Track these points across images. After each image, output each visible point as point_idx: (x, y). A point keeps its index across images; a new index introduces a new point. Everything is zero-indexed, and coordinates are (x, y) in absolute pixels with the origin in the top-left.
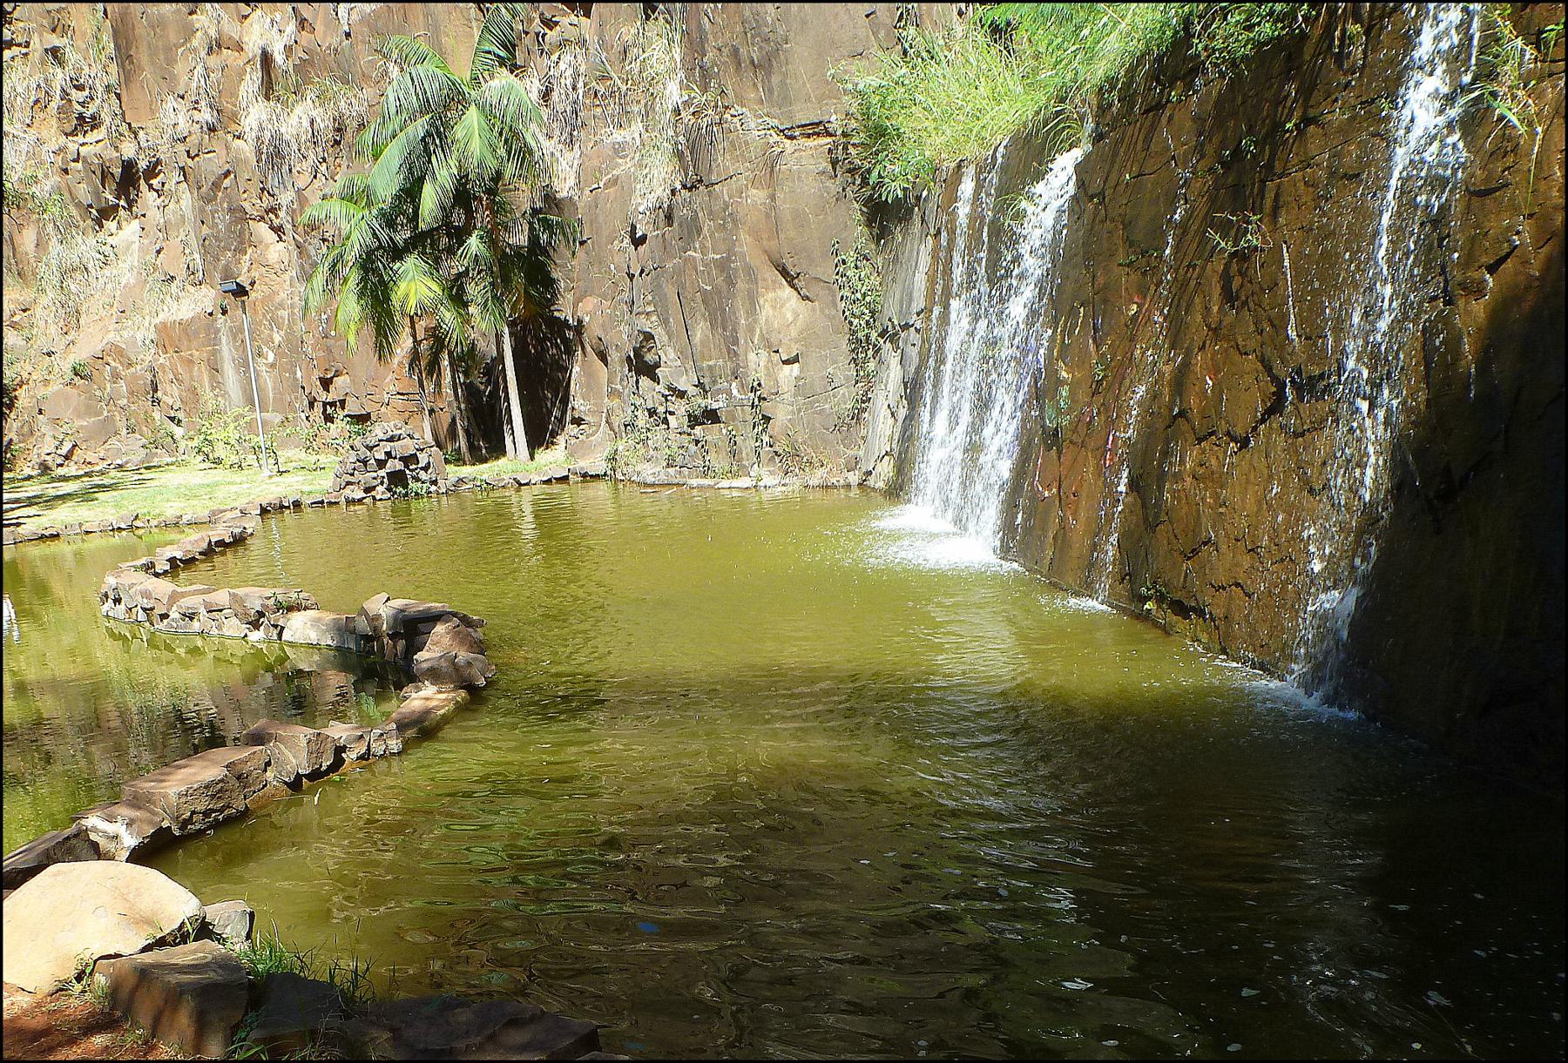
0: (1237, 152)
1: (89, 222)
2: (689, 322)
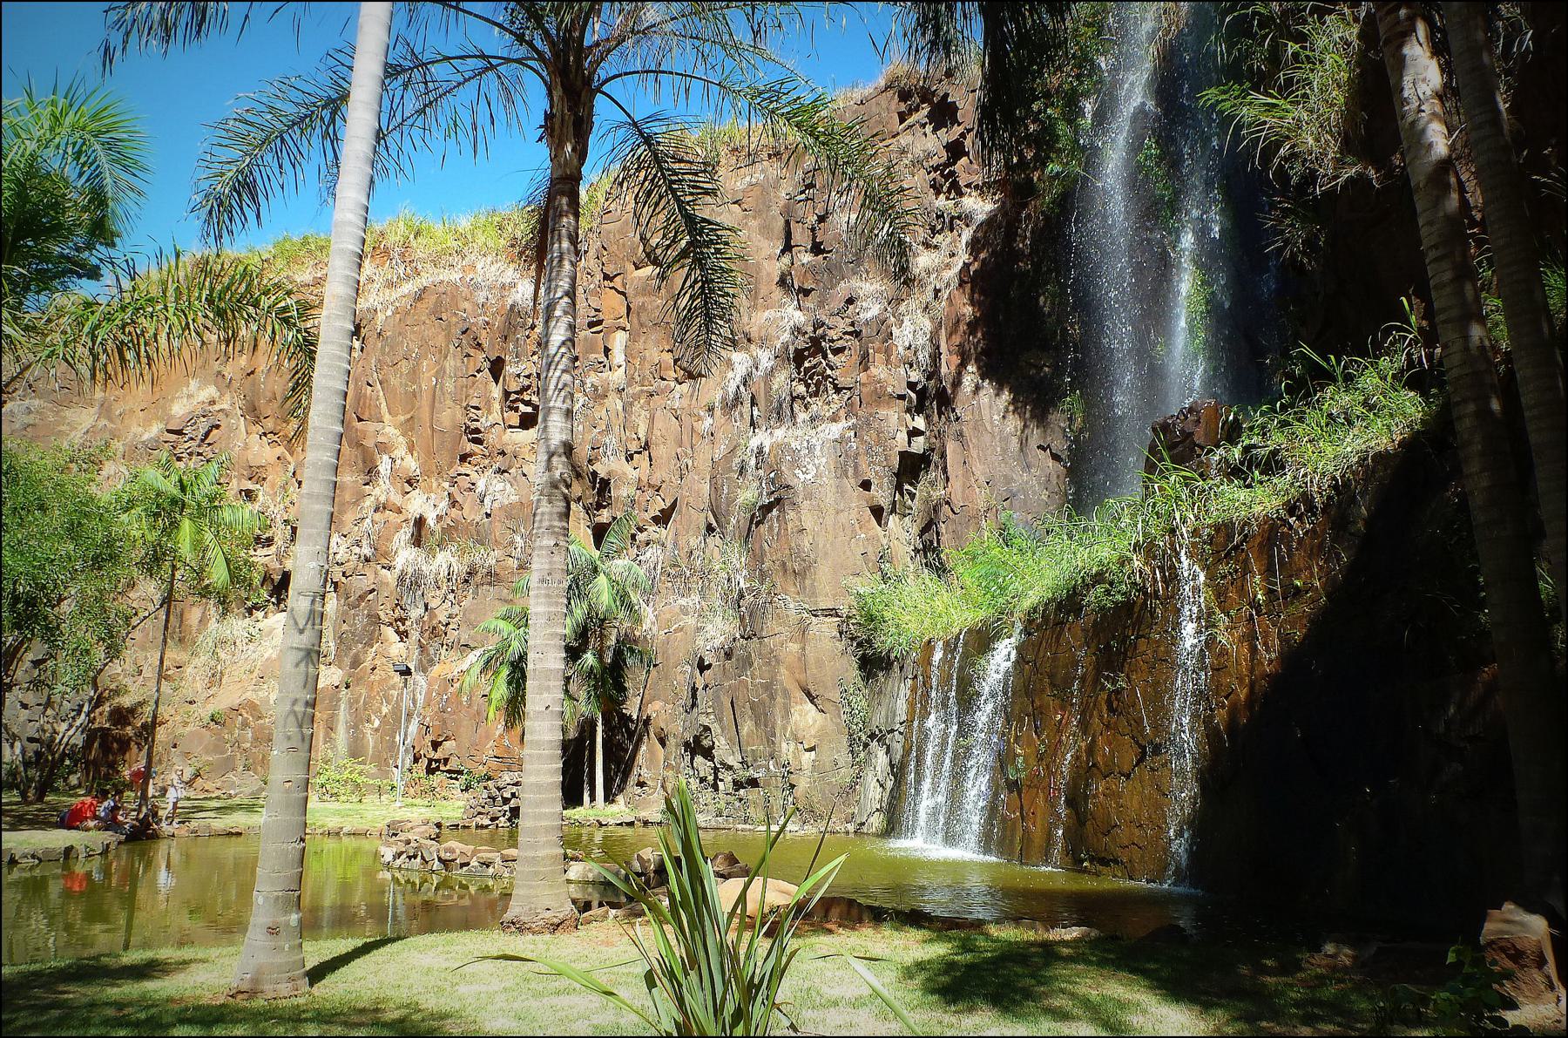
1: (242, 610)
2: (738, 720)
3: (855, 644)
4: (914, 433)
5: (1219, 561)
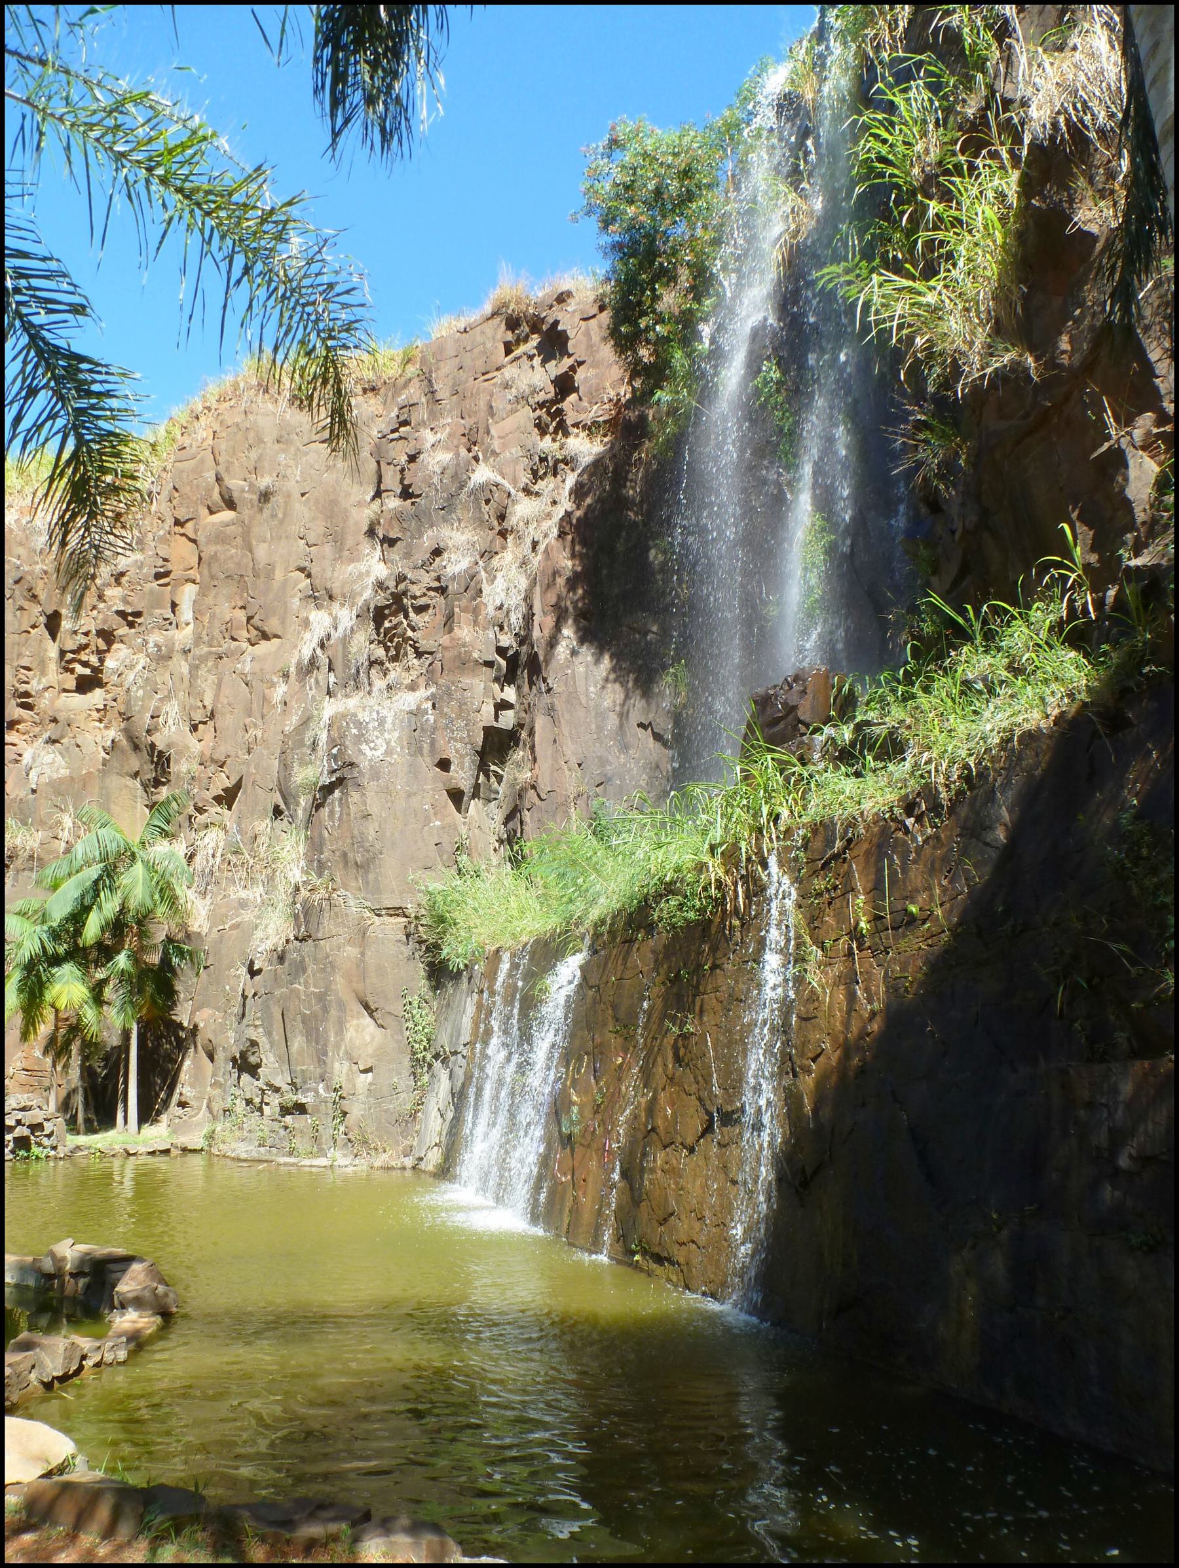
0: (678, 975)
2: (289, 1035)
3: (424, 948)
4: (502, 706)
5: (815, 873)
